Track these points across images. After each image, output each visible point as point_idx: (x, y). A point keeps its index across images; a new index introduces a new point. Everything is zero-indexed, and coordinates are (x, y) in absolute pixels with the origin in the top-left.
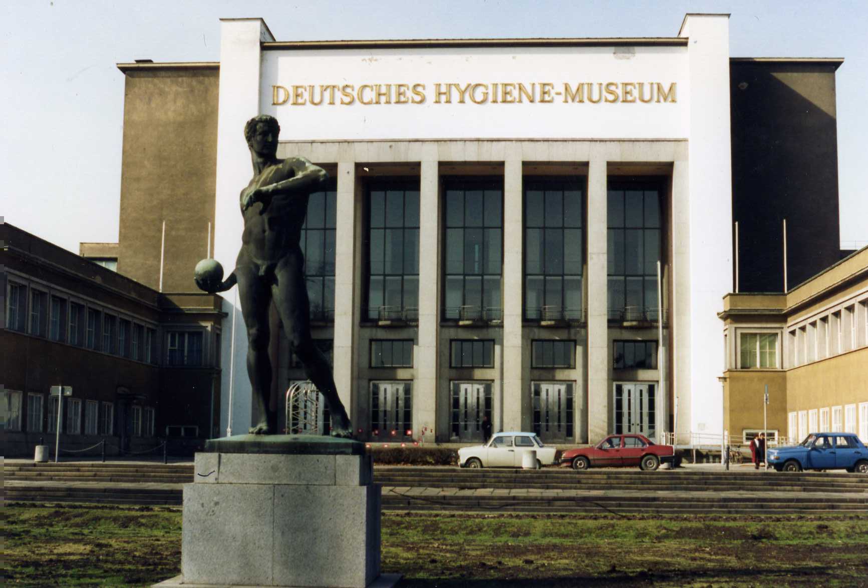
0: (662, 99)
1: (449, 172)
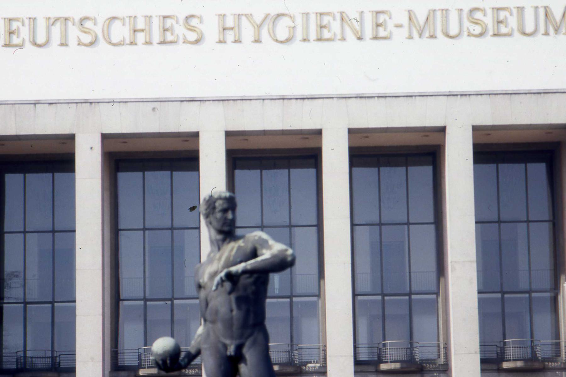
0: (551, 31)
1: (239, 145)
